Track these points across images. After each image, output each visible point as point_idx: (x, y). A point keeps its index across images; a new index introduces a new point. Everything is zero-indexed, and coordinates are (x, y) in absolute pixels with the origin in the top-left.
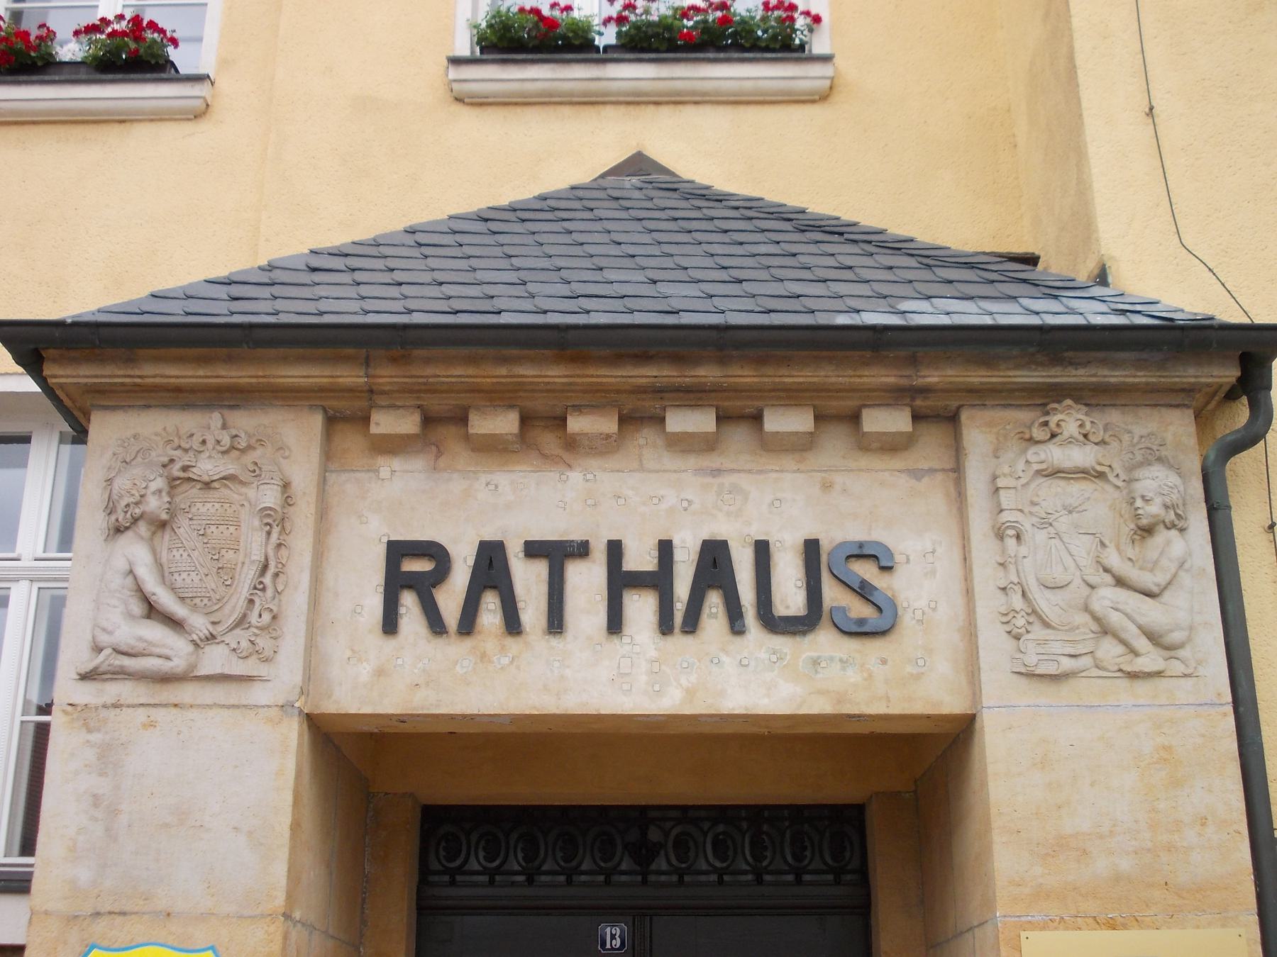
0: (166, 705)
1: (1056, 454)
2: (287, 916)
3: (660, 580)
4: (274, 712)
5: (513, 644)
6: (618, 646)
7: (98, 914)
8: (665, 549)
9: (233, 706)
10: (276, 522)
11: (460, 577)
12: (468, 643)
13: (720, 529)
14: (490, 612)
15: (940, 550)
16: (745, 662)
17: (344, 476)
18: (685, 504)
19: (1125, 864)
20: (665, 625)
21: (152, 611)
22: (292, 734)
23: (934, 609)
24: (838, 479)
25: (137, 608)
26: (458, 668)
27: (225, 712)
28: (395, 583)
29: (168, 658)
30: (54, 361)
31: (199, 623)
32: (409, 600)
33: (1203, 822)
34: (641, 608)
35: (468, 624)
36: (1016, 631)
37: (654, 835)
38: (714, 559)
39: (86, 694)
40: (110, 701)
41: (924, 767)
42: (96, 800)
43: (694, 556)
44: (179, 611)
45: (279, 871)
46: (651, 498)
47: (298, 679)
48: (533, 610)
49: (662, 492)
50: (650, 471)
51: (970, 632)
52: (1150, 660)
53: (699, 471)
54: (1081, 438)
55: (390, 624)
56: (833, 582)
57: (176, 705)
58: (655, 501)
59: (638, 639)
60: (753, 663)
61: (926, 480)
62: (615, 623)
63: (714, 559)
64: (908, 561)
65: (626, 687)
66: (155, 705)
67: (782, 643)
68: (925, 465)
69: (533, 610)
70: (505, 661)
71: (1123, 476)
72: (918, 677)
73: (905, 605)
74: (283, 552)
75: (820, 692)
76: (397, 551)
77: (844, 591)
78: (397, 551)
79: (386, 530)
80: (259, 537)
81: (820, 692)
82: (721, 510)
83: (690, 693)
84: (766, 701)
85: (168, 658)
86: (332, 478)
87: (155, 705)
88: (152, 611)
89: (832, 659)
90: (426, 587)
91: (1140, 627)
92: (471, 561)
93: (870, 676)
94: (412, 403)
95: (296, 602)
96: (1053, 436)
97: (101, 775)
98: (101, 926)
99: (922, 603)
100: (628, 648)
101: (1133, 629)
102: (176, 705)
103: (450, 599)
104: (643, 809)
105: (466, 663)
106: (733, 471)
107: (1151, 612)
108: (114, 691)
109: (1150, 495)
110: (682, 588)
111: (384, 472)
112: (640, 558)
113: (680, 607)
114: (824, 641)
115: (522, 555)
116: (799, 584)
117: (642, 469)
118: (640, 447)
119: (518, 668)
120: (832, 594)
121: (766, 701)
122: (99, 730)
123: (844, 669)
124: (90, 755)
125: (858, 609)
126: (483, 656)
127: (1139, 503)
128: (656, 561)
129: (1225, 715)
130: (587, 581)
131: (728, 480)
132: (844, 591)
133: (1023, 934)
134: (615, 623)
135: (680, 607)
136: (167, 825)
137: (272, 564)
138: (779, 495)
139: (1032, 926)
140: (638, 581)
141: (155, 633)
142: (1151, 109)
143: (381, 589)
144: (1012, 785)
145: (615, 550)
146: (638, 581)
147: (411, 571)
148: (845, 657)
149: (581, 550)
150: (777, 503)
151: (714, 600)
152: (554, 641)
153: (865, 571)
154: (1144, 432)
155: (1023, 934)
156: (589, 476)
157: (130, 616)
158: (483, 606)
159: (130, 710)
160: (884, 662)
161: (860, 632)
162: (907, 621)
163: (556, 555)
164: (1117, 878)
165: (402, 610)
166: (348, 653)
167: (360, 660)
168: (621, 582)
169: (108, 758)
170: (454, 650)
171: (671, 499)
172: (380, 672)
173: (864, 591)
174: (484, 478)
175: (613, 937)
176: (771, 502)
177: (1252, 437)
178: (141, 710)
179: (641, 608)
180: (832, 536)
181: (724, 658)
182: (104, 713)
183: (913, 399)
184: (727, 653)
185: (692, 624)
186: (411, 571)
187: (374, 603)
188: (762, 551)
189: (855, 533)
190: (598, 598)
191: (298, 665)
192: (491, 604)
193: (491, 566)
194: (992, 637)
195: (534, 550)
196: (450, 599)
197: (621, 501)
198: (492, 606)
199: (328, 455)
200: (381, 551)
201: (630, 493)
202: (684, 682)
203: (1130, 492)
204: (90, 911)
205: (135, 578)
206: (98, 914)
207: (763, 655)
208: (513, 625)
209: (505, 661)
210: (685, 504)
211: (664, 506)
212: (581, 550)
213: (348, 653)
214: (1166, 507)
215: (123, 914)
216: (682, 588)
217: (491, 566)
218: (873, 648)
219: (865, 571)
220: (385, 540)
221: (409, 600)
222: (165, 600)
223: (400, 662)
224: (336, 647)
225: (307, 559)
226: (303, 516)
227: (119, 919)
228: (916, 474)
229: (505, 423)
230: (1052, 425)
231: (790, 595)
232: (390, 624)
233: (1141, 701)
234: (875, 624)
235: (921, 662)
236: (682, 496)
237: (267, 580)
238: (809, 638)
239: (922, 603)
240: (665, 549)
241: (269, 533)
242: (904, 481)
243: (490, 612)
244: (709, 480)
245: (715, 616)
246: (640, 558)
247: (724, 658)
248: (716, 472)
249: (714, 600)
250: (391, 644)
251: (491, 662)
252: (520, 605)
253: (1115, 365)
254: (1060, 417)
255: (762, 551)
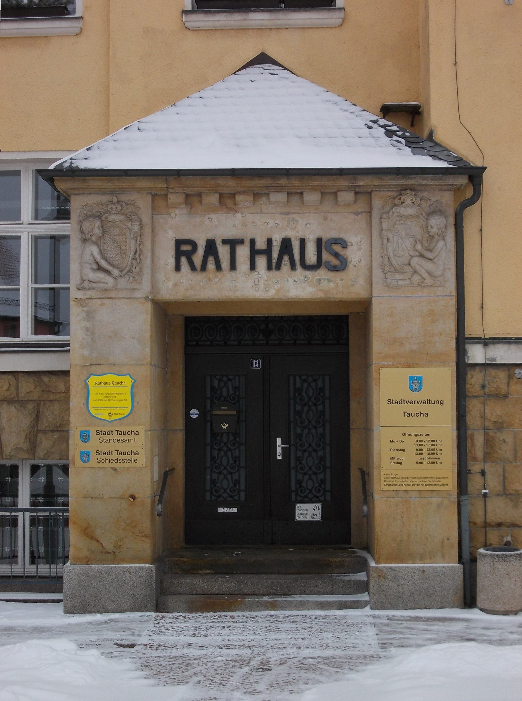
0: (107, 298)
1: (402, 210)
2: (151, 364)
3: (268, 252)
4: (143, 300)
5: (219, 274)
6: (254, 275)
7: (91, 365)
8: (270, 242)
9: (129, 298)
10: (139, 237)
11: (201, 252)
12: (204, 274)
13: (290, 234)
14: (211, 265)
15: (363, 241)
16: (296, 280)
17: (159, 216)
18: (276, 225)
19: (415, 347)
20: (269, 267)
21: (100, 268)
22: (149, 306)
23: (360, 262)
24: (329, 216)
25: (95, 266)
26: (201, 283)
27: (126, 300)
28: (179, 254)
29: (107, 283)
30: (58, 180)
31: (116, 272)
32: (184, 260)
33: (441, 334)
34: (261, 262)
35: (204, 268)
36: (385, 272)
37: (271, 326)
38: (286, 244)
39: (80, 295)
40: (88, 297)
41: (363, 308)
42: (87, 329)
43: (279, 244)
44: (109, 268)
45: (148, 350)
46: (265, 223)
47: (149, 289)
48: (225, 263)
49: (269, 221)
50: (264, 213)
51: (371, 270)
52: (429, 281)
53: (281, 213)
54: (412, 204)
55: (178, 268)
56: (327, 252)
57: (110, 298)
58: (266, 224)
59: (260, 273)
60: (299, 281)
61: (360, 216)
62: (253, 267)
63: (286, 244)
64: (352, 245)
65: (257, 289)
66: (103, 298)
67: (308, 273)
68: (359, 210)
69: (225, 263)
70: (217, 280)
71: (425, 217)
72: (353, 285)
73: (350, 260)
74: (141, 246)
75: (320, 290)
76: (179, 243)
77: (330, 255)
78: (179, 243)
79: (174, 236)
80: (133, 242)
81: (320, 290)
82: (289, 227)
83: (278, 291)
84: (302, 293)
85: (107, 283)
86: (155, 217)
87: (103, 298)
88: (100, 268)
89: (325, 279)
90: (189, 256)
91: (426, 270)
92: (204, 246)
93: (337, 284)
94: (182, 191)
95: (148, 262)
96: (402, 203)
97: (88, 321)
98: (93, 368)
99: (356, 260)
100: (257, 276)
101: (424, 271)
102: (110, 298)
103: (198, 258)
104: (267, 318)
105: (204, 281)
106: (294, 213)
107: (429, 266)
108: (90, 294)
109: (433, 225)
110: (275, 255)
111: (173, 215)
112: (261, 245)
113: (274, 262)
114: (322, 273)
115: (221, 244)
116: (315, 253)
117: (261, 212)
118: (261, 204)
119: (221, 283)
120: (326, 256)
121: (302, 293)
122: (86, 307)
123: (329, 283)
124: (84, 314)
125: (335, 262)
126: (210, 279)
127: (429, 228)
128: (266, 246)
129: (452, 299)
130: (243, 253)
131: (291, 216)
132: (330, 255)
133: (381, 369)
134: (253, 267)
135: (274, 262)
136: (111, 337)
137: (138, 250)
138: (309, 222)
139: (384, 366)
140: (260, 252)
141: (101, 275)
142: (456, 63)
143: (174, 256)
144: (379, 322)
145: (253, 242)
146: (260, 252)
147: (184, 250)
148: (329, 278)
149: (242, 242)
150: (308, 225)
151: (286, 259)
152: (233, 273)
153: (337, 248)
154: (435, 200)
155: (381, 369)
156: (244, 215)
157: (93, 269)
158: (208, 262)
159: (96, 300)
160: (342, 280)
161: (334, 269)
162: (350, 266)
163: (233, 243)
164: (412, 351)
165: (182, 264)
166: (165, 279)
167: (168, 281)
168: (254, 253)
169: (90, 316)
170: (199, 277)
171: (272, 223)
172: (175, 285)
173: (336, 255)
174: (207, 217)
175: (256, 363)
176: (306, 226)
177: (472, 201)
178: (99, 300)
179: (261, 262)
180: (326, 236)
181: (289, 279)
182: (87, 301)
183: (355, 189)
184: (290, 277)
185: (278, 267)
186: (184, 250)
187: (172, 261)
188: (303, 242)
189: (334, 235)
190: (247, 258)
191: (149, 284)
192: (211, 260)
193: (211, 247)
194: (377, 273)
195: (225, 242)
196: (198, 258)
197: (255, 224)
198: (211, 262)
199: (154, 209)
200: (172, 244)
201: (258, 221)
202: (276, 287)
203: (427, 223)
204: (89, 364)
205: (94, 257)
206: (91, 365)
207: (302, 278)
208: (219, 267)
209: (217, 280)
210: (276, 225)
211: (269, 226)
212: (242, 242)
213: (165, 279)
214: (438, 229)
215: (100, 364)
216: (275, 255)
217: (211, 247)
218: (338, 276)
219: (337, 248)
220: (174, 239)
221: (184, 260)
222: (103, 263)
223: (182, 281)
224: (161, 277)
225: (149, 248)
226: (147, 230)
227: (99, 366)
228: (356, 214)
229: (213, 199)
230: (402, 199)
231: (311, 257)
232: (178, 268)
233: (424, 295)
234: (341, 265)
235: (354, 280)
236: (276, 222)
237: (137, 256)
238: (318, 271)
239: (356, 260)
240: (270, 242)
241: (136, 240)
242: (352, 216)
243: (211, 265)
244: (285, 216)
245: (285, 265)
246: (261, 245)
247: (289, 279)
248: (287, 214)
249: (286, 259)
250: (179, 275)
251: (212, 281)
252: (221, 261)
253: (424, 179)
254: (404, 196)
255: (303, 242)
